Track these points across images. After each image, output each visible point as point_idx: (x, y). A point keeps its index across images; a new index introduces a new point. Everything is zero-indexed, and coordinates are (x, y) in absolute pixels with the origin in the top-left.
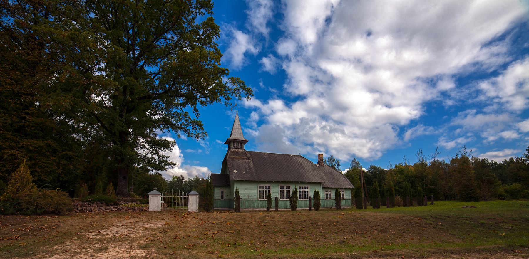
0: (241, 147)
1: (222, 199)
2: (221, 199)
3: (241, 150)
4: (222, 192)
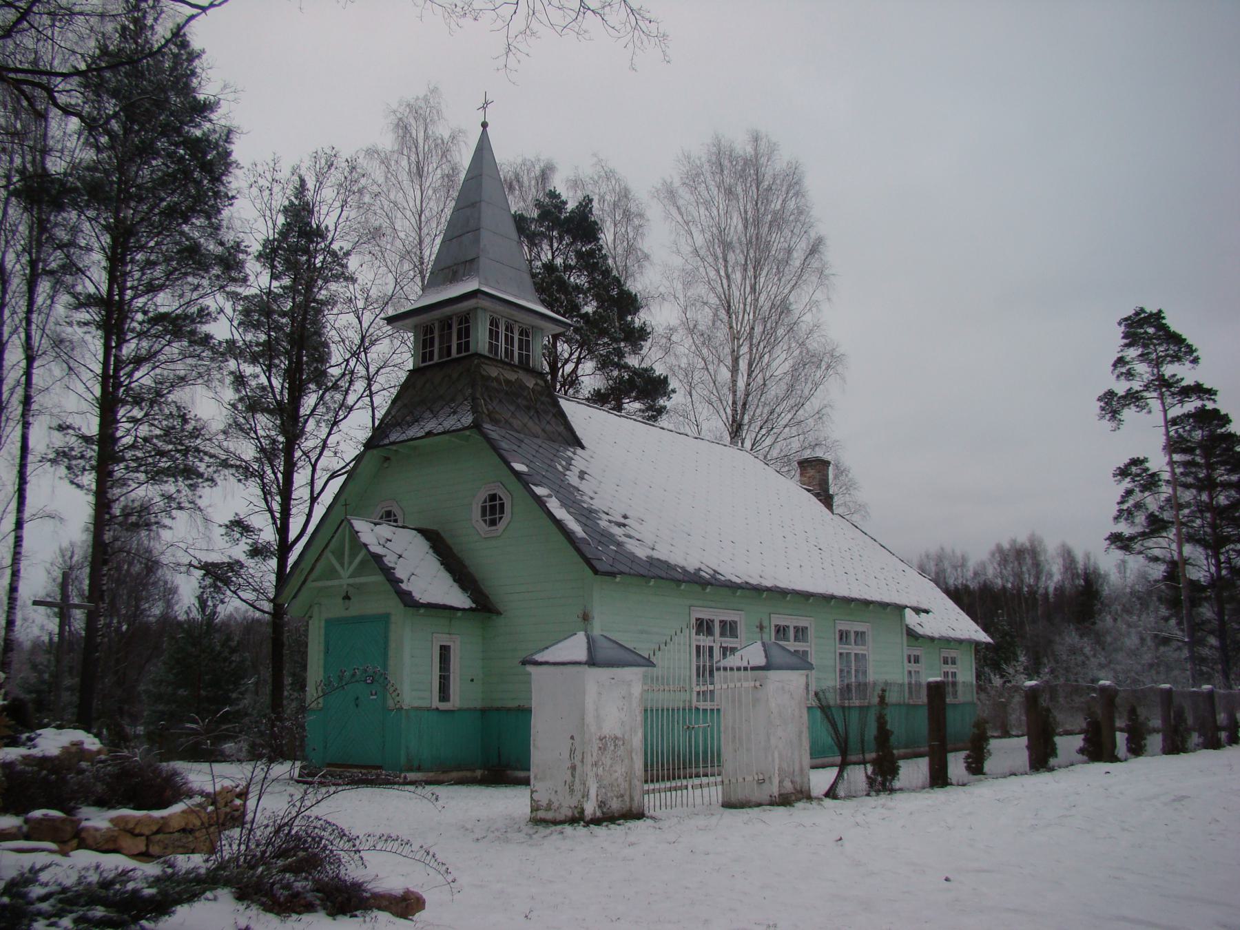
0: (528, 356)
2: (436, 703)
4: (445, 651)
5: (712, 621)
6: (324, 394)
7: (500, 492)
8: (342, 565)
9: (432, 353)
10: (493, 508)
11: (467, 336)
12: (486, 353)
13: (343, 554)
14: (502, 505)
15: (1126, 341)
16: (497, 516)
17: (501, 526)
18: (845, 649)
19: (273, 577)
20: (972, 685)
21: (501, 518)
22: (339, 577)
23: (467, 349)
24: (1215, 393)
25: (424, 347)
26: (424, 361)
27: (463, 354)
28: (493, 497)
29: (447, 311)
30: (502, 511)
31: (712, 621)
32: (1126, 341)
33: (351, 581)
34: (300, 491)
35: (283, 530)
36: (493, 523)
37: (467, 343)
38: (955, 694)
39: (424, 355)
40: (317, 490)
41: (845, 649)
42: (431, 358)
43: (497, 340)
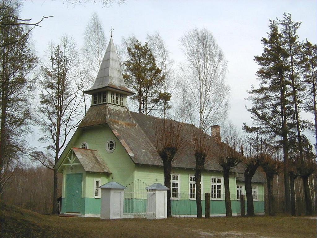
1: (96, 197)
3: (123, 110)
5: (215, 179)
6: (59, 91)
7: (113, 141)
8: (71, 159)
9: (96, 101)
10: (111, 145)
11: (105, 97)
12: (111, 103)
13: (71, 156)
14: (113, 144)
15: (200, 34)
16: (110, 144)
17: (113, 150)
18: (214, 184)
19: (54, 159)
20: (262, 196)
21: (113, 148)
22: (70, 163)
23: (105, 101)
24: (262, 54)
25: (94, 100)
26: (94, 104)
27: (104, 103)
28: (111, 142)
29: (101, 90)
30: (113, 146)
31: (215, 179)
32: (200, 34)
33: (73, 164)
34: (62, 132)
35: (57, 144)
36: (111, 149)
37: (105, 100)
38: (256, 198)
39: (94, 102)
40: (67, 134)
41: (214, 184)
42: (96, 103)
43: (113, 99)
